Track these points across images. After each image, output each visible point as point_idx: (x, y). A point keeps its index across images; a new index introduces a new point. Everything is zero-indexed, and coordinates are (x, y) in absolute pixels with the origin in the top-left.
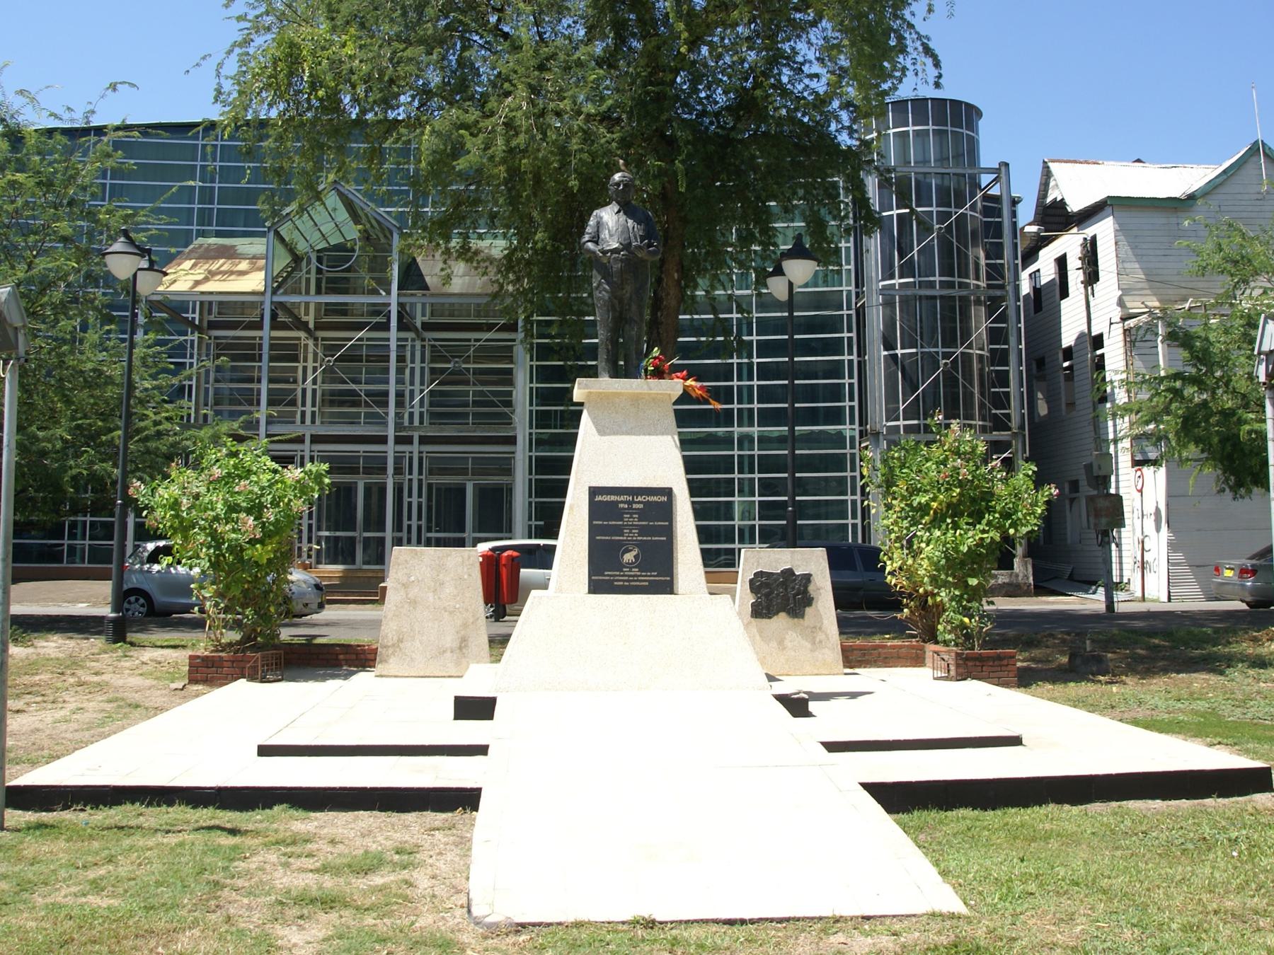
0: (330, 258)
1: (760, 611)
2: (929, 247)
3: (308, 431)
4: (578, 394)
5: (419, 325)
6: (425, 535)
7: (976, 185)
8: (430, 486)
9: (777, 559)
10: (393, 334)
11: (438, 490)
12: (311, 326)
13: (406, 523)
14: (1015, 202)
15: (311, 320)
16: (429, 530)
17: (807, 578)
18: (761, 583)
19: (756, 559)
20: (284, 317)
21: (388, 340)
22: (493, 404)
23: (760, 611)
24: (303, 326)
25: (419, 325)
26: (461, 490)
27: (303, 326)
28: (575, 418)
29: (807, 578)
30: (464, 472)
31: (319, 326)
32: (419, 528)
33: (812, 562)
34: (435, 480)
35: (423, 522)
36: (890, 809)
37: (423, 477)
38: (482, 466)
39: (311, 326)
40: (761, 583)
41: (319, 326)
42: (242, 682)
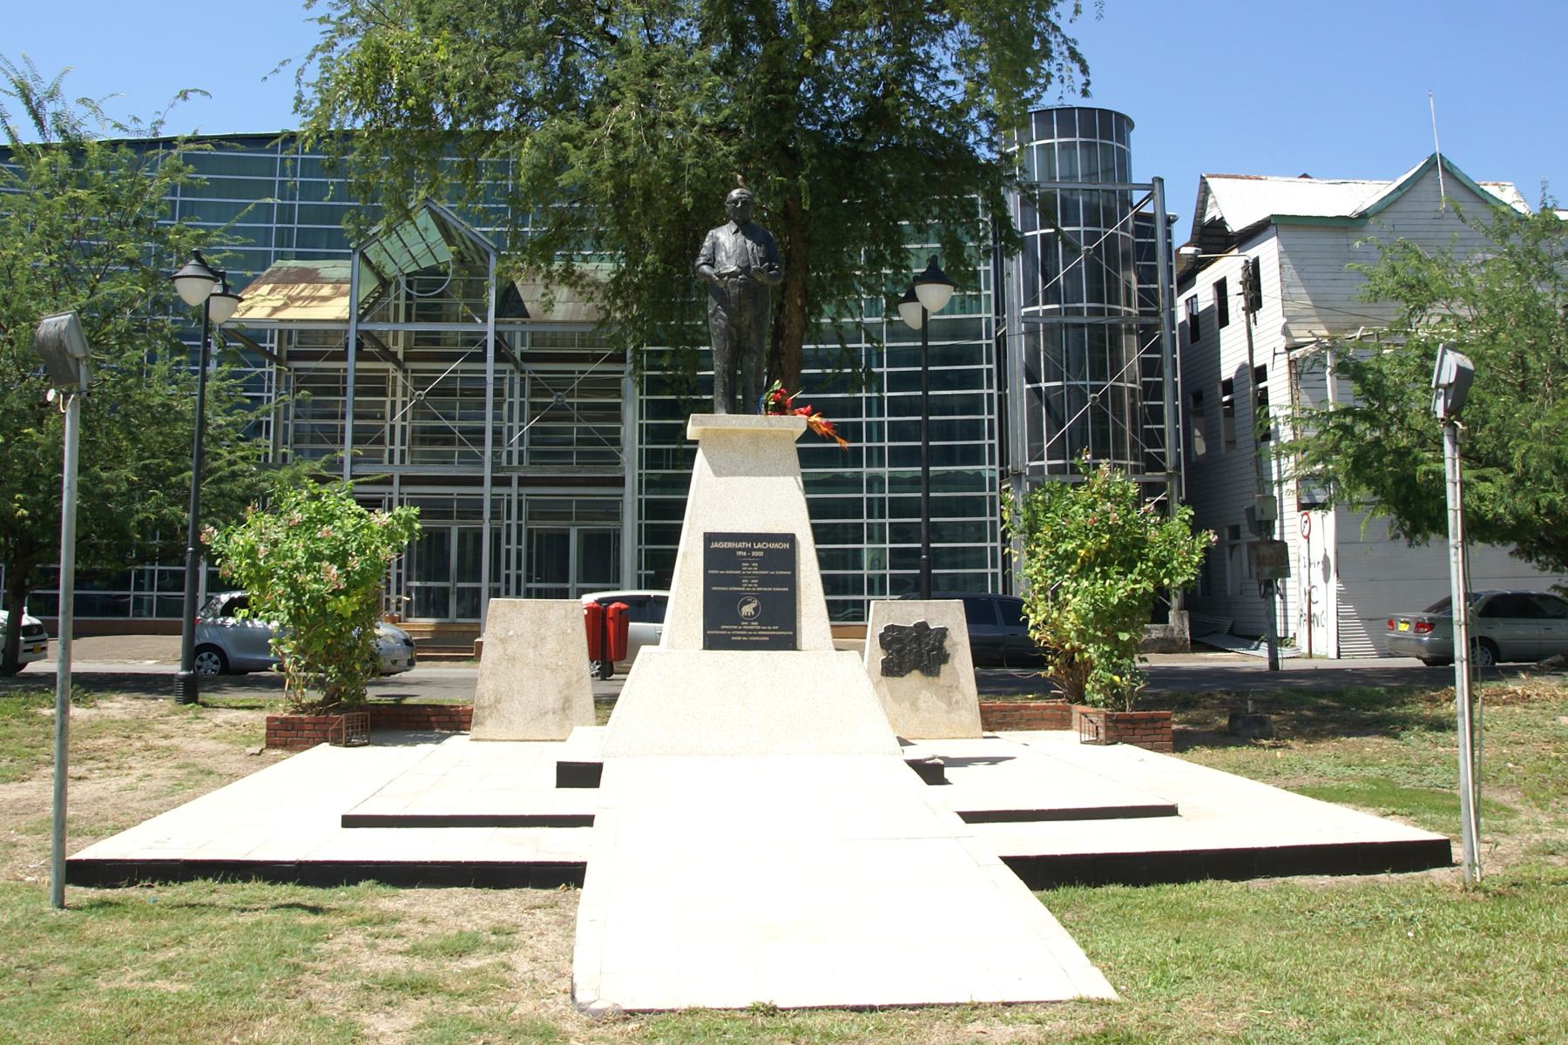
2: (1077, 269)
5: (518, 355)
6: (525, 585)
8: (530, 531)
10: (490, 365)
12: (400, 356)
13: (503, 572)
15: (399, 350)
16: (529, 580)
17: (943, 632)
20: (371, 347)
21: (484, 372)
24: (392, 357)
25: (518, 355)
26: (565, 537)
29: (943, 632)
30: (567, 516)
31: (409, 357)
32: (519, 578)
34: (536, 525)
35: (523, 572)
38: (590, 510)
39: (400, 356)
41: (409, 357)
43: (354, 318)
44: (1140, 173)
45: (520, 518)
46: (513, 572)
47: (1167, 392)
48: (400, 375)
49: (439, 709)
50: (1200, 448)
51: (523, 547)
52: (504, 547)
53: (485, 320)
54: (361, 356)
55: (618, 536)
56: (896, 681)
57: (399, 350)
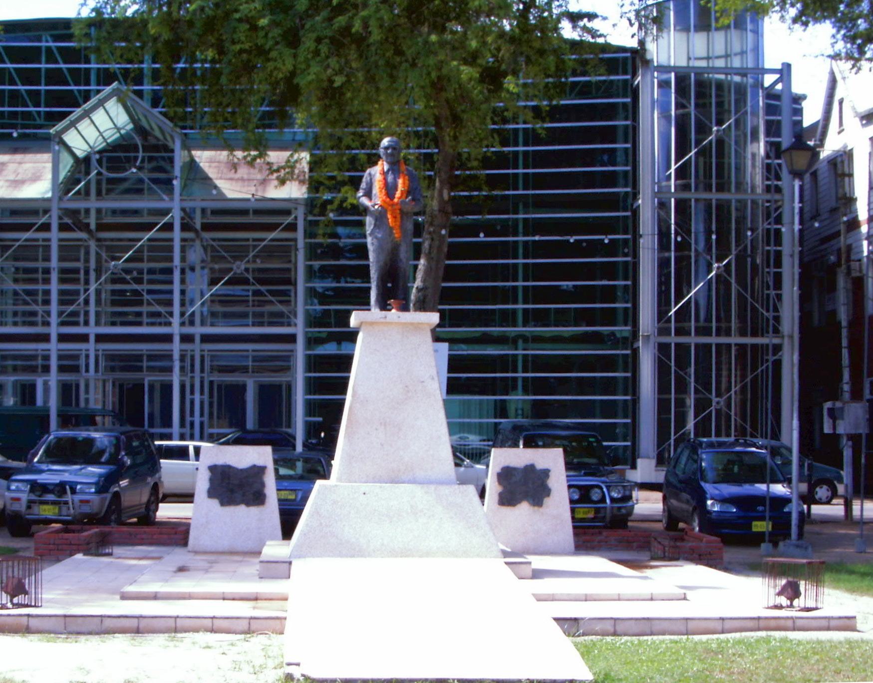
0: (109, 159)
1: (508, 499)
2: (687, 164)
3: (92, 330)
4: (354, 320)
5: (198, 226)
6: (208, 431)
7: (759, 84)
8: (211, 382)
9: (518, 456)
10: (177, 234)
11: (219, 386)
12: (93, 226)
13: (188, 419)
14: (798, 99)
15: (92, 222)
16: (211, 426)
17: (546, 473)
18: (506, 475)
19: (501, 457)
20: (73, 221)
21: (171, 240)
22: (271, 292)
23: (508, 499)
24: (86, 227)
25: (198, 226)
26: (243, 388)
27: (86, 227)
28: (352, 337)
29: (546, 473)
30: (244, 370)
31: (101, 227)
32: (202, 424)
33: (551, 460)
34: (217, 378)
35: (206, 419)
36: (568, 633)
37: (205, 375)
38: (264, 363)
39: (93, 226)
40: (506, 475)
41: (101, 227)
42: (79, 556)
43: (57, 199)
44: (772, 61)
45: (202, 371)
46: (197, 420)
47: (786, 261)
48: (93, 244)
49: (833, 234)
50: (135, 520)
51: (206, 397)
52: (188, 396)
53: (172, 200)
54: (63, 227)
55: (290, 387)
56: (507, 511)
57: (92, 222)
